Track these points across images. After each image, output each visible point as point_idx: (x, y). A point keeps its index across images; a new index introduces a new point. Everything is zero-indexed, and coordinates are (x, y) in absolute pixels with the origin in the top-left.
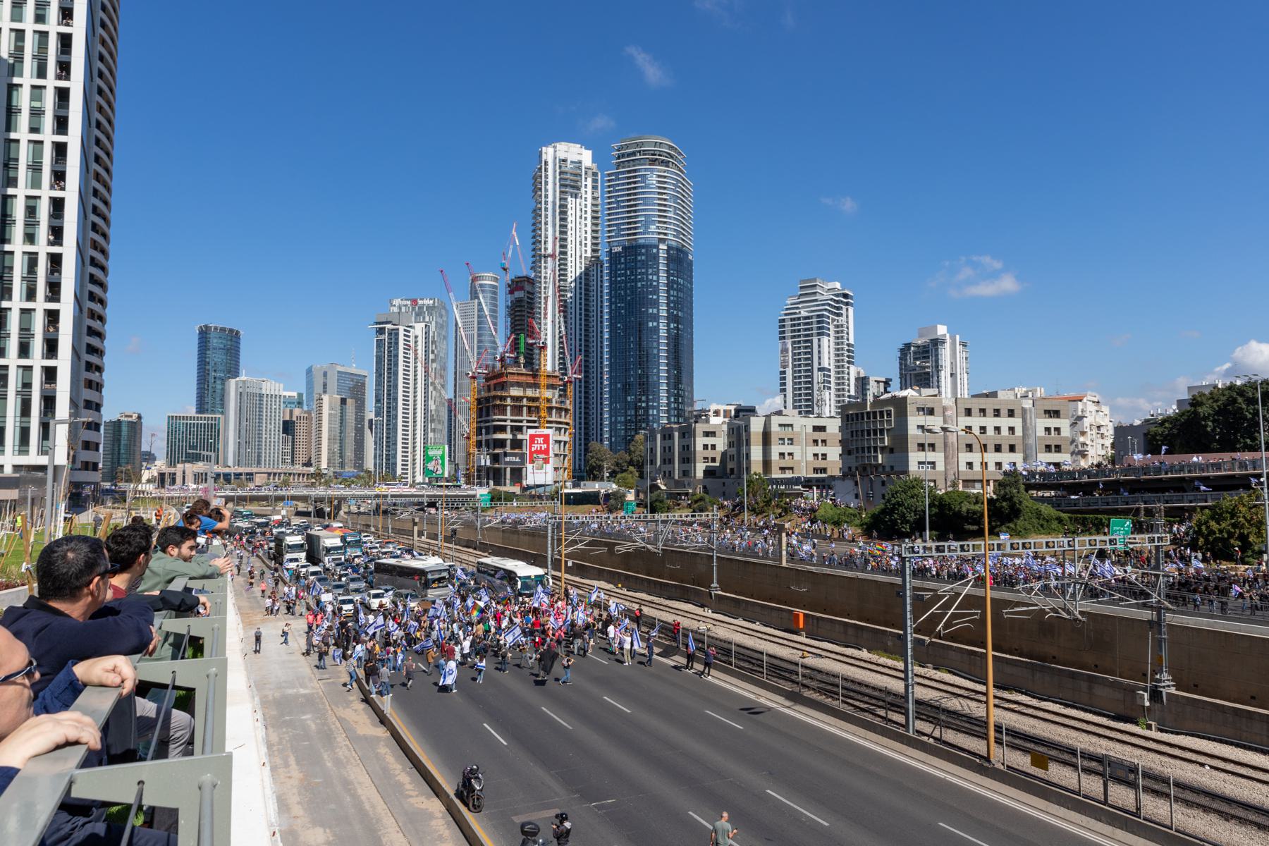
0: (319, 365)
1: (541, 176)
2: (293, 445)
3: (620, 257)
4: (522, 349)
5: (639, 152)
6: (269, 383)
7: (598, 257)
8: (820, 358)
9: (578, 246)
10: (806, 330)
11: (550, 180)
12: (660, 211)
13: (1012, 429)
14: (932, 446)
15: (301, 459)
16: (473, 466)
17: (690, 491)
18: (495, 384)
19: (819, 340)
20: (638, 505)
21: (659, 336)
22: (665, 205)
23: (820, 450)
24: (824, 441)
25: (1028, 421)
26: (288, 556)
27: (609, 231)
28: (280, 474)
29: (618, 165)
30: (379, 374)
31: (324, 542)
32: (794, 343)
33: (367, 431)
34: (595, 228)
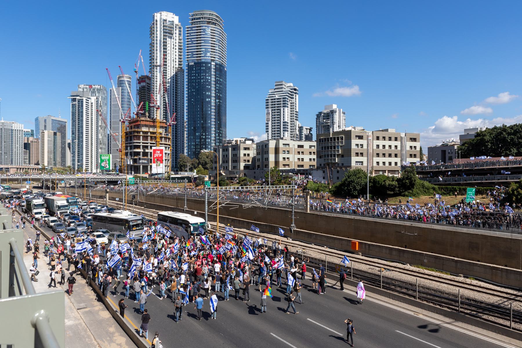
0: (42, 116)
1: (154, 27)
2: (29, 155)
3: (193, 67)
4: (147, 109)
5: (202, 18)
6: (16, 124)
7: (181, 68)
8: (284, 117)
9: (172, 62)
10: (278, 104)
11: (159, 29)
12: (212, 46)
13: (396, 147)
14: (362, 154)
15: (33, 162)
16: (124, 165)
17: (237, 176)
18: (134, 125)
19: (284, 109)
20: (211, 183)
21: (211, 105)
22: (214, 44)
23: (301, 156)
24: (302, 152)
25: (403, 143)
26: (35, 211)
27: (188, 55)
28: (23, 169)
29: (192, 24)
30: (74, 121)
31: (57, 203)
32: (272, 110)
33: (67, 149)
34: (180, 54)
